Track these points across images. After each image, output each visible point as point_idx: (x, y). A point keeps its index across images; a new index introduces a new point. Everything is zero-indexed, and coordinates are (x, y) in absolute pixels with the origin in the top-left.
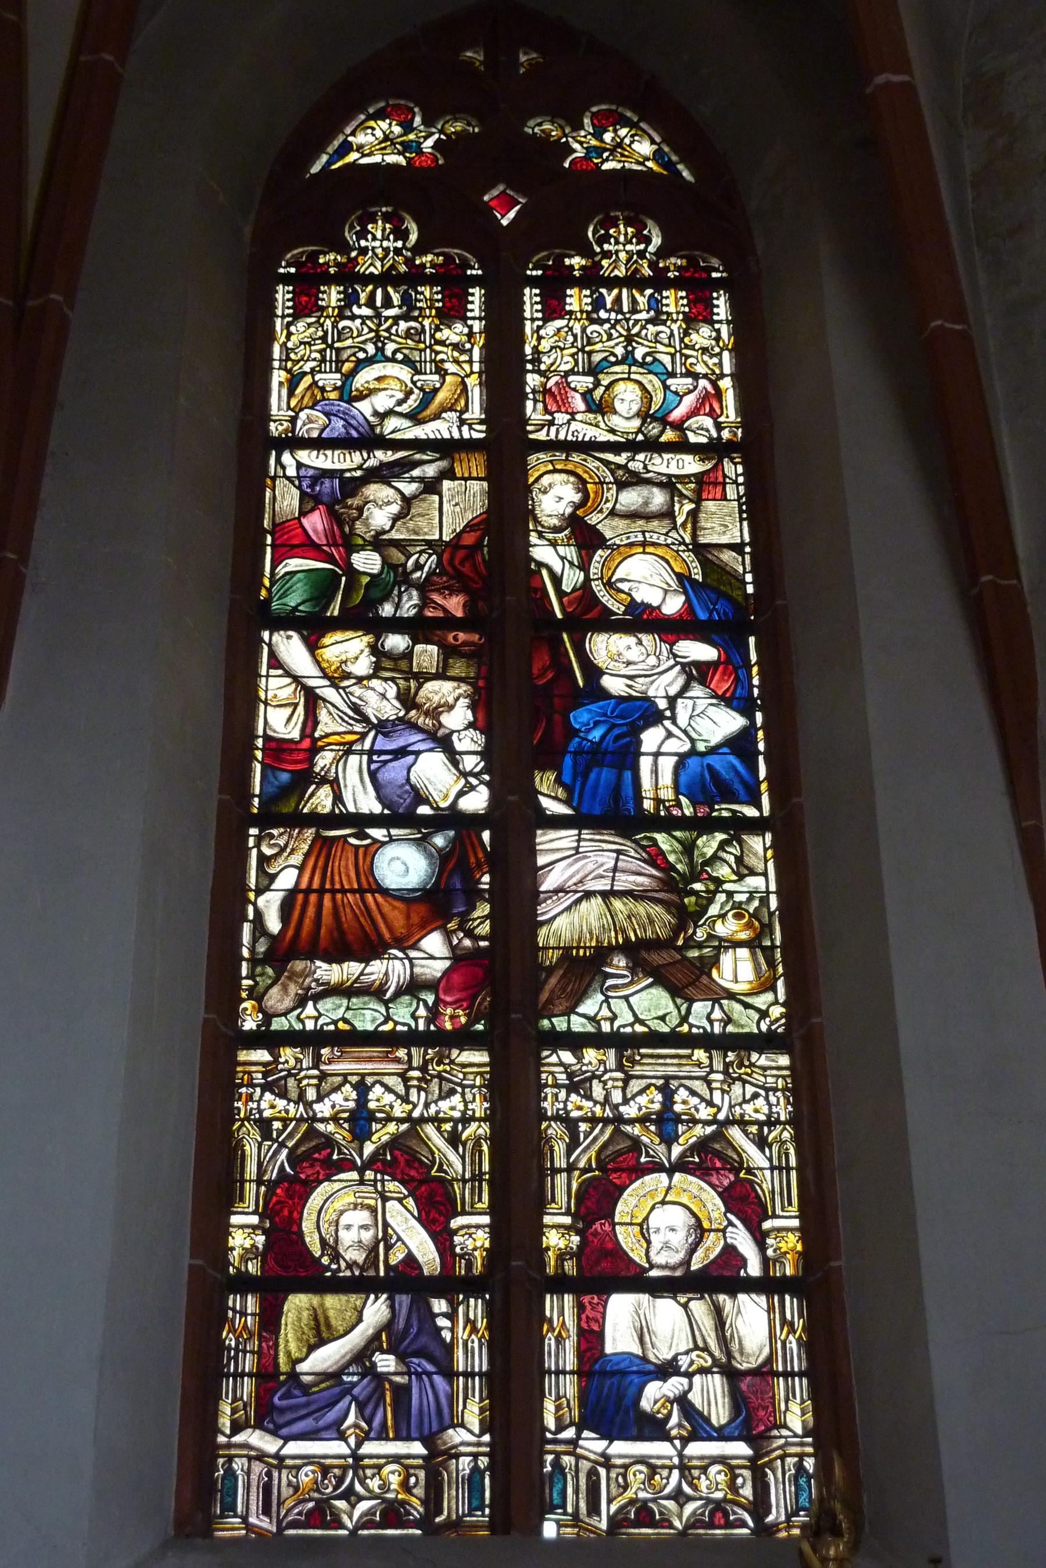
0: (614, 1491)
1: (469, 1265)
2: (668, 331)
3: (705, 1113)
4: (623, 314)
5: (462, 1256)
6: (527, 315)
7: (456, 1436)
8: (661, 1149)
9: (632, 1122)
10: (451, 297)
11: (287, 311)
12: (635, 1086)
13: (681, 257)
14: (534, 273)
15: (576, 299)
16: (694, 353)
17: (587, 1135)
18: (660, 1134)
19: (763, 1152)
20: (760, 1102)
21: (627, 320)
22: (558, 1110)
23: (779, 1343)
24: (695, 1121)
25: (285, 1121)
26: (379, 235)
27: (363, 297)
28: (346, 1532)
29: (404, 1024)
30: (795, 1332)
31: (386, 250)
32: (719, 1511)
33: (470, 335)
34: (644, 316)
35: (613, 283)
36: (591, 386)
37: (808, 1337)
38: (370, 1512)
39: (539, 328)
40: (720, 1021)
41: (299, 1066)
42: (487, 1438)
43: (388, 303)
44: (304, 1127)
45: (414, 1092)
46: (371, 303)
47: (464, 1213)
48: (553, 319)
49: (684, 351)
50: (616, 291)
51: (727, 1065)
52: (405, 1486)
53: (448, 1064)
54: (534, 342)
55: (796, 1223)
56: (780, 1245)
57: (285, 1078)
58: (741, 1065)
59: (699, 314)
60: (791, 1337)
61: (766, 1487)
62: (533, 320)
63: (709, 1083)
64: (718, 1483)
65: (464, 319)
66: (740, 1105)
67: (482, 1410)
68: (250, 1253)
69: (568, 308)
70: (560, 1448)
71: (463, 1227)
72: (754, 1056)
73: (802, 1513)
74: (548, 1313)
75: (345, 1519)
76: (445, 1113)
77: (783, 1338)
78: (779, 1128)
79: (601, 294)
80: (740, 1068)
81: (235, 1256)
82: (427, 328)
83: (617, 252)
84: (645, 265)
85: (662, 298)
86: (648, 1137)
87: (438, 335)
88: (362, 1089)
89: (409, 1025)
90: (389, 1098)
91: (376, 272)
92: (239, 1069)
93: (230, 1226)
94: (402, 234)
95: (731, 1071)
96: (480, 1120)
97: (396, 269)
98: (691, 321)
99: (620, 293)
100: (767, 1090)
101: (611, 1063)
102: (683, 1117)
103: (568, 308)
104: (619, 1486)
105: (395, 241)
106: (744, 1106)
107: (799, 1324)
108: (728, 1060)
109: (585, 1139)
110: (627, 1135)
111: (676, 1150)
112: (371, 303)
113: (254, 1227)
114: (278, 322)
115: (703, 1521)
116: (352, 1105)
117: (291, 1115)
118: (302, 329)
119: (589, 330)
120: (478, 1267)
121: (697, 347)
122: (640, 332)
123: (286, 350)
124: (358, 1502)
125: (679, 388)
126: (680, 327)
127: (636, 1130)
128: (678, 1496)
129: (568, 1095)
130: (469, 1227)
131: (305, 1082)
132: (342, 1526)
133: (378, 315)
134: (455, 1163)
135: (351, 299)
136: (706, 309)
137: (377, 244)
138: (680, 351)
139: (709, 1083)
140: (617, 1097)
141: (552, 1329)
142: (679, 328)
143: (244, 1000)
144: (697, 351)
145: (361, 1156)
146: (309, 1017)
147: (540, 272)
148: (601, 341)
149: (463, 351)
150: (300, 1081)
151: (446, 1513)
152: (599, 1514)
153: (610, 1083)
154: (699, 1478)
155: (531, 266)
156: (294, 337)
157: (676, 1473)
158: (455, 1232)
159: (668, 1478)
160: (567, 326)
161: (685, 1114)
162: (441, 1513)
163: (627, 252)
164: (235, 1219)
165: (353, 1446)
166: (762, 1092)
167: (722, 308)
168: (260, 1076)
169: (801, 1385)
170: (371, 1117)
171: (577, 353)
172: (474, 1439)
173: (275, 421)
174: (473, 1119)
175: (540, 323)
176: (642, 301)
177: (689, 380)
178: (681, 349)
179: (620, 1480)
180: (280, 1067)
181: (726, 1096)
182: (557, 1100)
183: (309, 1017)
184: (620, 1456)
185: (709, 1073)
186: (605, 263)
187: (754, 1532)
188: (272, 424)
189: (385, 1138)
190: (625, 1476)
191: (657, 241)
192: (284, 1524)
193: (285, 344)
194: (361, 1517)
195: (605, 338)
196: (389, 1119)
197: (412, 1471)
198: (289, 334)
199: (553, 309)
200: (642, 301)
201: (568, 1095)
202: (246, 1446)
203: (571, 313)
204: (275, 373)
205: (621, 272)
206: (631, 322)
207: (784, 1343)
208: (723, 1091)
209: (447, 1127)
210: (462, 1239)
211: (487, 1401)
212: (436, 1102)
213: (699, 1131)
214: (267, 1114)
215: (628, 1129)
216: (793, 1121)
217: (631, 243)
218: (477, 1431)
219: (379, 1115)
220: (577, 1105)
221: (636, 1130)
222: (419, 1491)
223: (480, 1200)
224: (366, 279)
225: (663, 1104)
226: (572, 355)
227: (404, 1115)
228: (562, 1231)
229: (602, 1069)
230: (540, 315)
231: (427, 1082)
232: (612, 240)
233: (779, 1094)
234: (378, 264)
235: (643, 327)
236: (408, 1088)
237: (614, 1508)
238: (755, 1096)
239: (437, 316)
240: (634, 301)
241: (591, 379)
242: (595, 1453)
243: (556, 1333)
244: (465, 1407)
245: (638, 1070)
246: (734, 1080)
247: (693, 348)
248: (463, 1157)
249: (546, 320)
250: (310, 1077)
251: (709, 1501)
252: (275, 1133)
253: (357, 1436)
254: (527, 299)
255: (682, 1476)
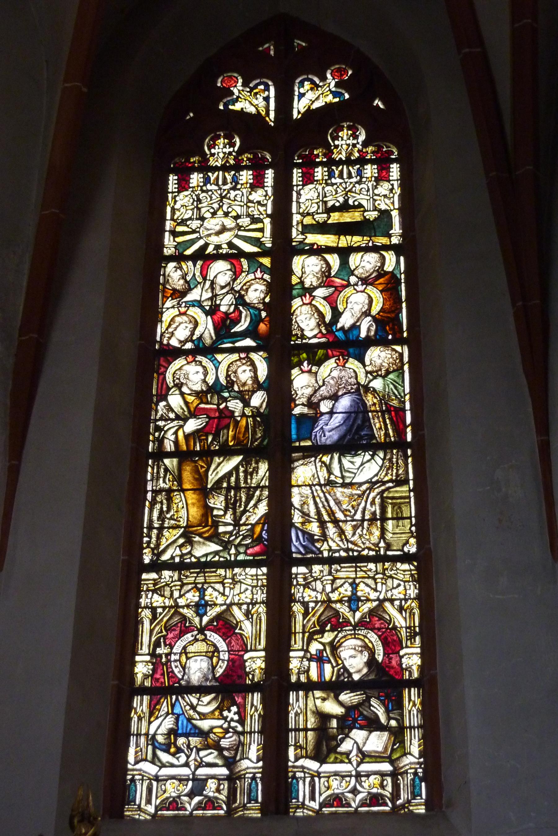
0: (323, 789)
1: (410, 674)
2: (241, 193)
3: (221, 600)
4: (343, 179)
5: (406, 669)
6: (295, 183)
7: (245, 764)
8: (197, 620)
9: (183, 607)
10: (311, 174)
11: (174, 190)
12: (339, 582)
13: (250, 154)
14: (298, 161)
15: (319, 173)
16: (253, 205)
17: (161, 614)
18: (350, 607)
19: (401, 613)
20: (401, 588)
21: (346, 183)
22: (147, 603)
23: (407, 711)
24: (216, 605)
25: (316, 602)
26: (345, 138)
27: (337, 173)
28: (353, 809)
29: (224, 558)
30: (257, 711)
31: (348, 145)
32: (375, 799)
33: (391, 190)
34: (354, 180)
35: (215, 169)
36: (326, 219)
37: (422, 707)
38: (200, 802)
39: (176, 196)
40: (384, 547)
41: (322, 575)
42: (260, 764)
43: (350, 176)
44: (172, 611)
45: (379, 585)
46: (341, 176)
47: (251, 650)
48: (183, 191)
49: (375, 197)
50: (217, 173)
51: (384, 570)
52: (218, 790)
53: (396, 570)
54: (172, 204)
55: (418, 650)
56: (409, 662)
57: (164, 586)
58: (392, 570)
59: (382, 177)
60: (255, 713)
61: (399, 785)
62: (297, 186)
63: (375, 579)
64: (374, 784)
65: (263, 187)
66: (238, 594)
67: (258, 750)
68: (146, 677)
69: (316, 178)
70: (135, 773)
71: (405, 655)
72: (399, 565)
73: (252, 802)
74: (135, 705)
75: (187, 806)
76: (243, 600)
77: (409, 709)
78: (258, 606)
79: (208, 176)
80: (391, 571)
81: (139, 677)
82: (245, 194)
83: (218, 153)
84: (356, 151)
85: (240, 175)
86: (343, 609)
87: (376, 192)
88: (354, 585)
89: (226, 558)
90: (367, 589)
91: (219, 165)
92: (142, 582)
93: (290, 657)
94: (232, 145)
95: (235, 578)
96: (260, 603)
97: (229, 163)
98: (378, 180)
99: (343, 168)
100: (405, 582)
101: (176, 577)
102: (209, 603)
103: (316, 178)
104: (325, 787)
105: (229, 148)
106: (393, 590)
107: (418, 701)
108: (234, 572)
109: (160, 616)
110: (181, 614)
111: (358, 615)
112: (341, 176)
113: (147, 662)
114: (170, 196)
115: (366, 803)
116: (349, 593)
117: (319, 599)
118: (307, 192)
119: (326, 189)
120: (416, 675)
121: (255, 201)
122: (352, 188)
123: (173, 210)
124: (359, 794)
125: (320, 219)
126: (373, 185)
127: (185, 611)
128: (354, 791)
129: (304, 589)
130: (409, 654)
131: (173, 588)
132: (351, 807)
133: (220, 189)
134: (399, 620)
135: (331, 175)
136: (386, 174)
137: (344, 142)
138: (372, 198)
139: (375, 579)
140: (328, 588)
141: (136, 713)
142: (247, 192)
143: (145, 548)
144: (255, 203)
145: (354, 619)
146: (325, 550)
147: (301, 161)
148: (332, 195)
149: (263, 205)
150: (171, 587)
151: (238, 802)
152: (151, 804)
153: (325, 582)
154: (365, 782)
155: (296, 158)
156: (180, 204)
157: (353, 779)
158: (246, 661)
159: (350, 782)
160: (315, 188)
161: (211, 601)
162: (236, 802)
163: (224, 153)
164: (138, 658)
165: (193, 770)
166: (402, 583)
167: (395, 170)
168: (152, 585)
169: (417, 733)
170: (358, 599)
171: (319, 202)
172: (416, 760)
173: (167, 248)
174: (256, 603)
175: (176, 194)
176: (353, 172)
177: (199, 222)
178: (247, 203)
179: (326, 784)
180: (162, 581)
181: (384, 585)
182: (147, 598)
183: (325, 550)
184: (325, 772)
185: (375, 575)
186: (211, 159)
187: (226, 812)
188: (165, 249)
189: (214, 614)
190: (328, 781)
191: (362, 137)
192: (158, 809)
193: (173, 207)
194: (360, 801)
195: (334, 193)
196: (368, 600)
197: (221, 782)
198: (175, 202)
199: (308, 179)
200: (353, 172)
201: (304, 589)
202: (303, 767)
203: (317, 181)
204: (294, 216)
205: (343, 156)
206: (348, 184)
207: (410, 712)
208: (231, 589)
209: (397, 603)
210: (249, 664)
211: (422, 741)
212: (391, 590)
213: (218, 609)
214: (306, 600)
215: (181, 610)
216: (418, 598)
217: (349, 139)
218: (417, 756)
219: (362, 598)
220: (157, 600)
221: (338, 606)
222: (225, 792)
223: (260, 644)
224: (215, 169)
225: (352, 591)
226: (317, 203)
227: (376, 598)
228: (144, 664)
229: (171, 580)
230: (301, 183)
231: (386, 580)
232: (340, 139)
233: (258, 588)
234: (220, 161)
235: (354, 186)
236: (376, 583)
237: (158, 801)
238: (399, 585)
239: (250, 187)
240: (225, 179)
241: (326, 215)
242: (152, 775)
243: (258, 712)
244: (411, 744)
245: (340, 575)
246: (237, 582)
247: (379, 195)
248: (405, 619)
249: (179, 192)
250: (327, 580)
251: (369, 793)
252: (158, 614)
253: (195, 765)
254: (170, 182)
255: (357, 781)
